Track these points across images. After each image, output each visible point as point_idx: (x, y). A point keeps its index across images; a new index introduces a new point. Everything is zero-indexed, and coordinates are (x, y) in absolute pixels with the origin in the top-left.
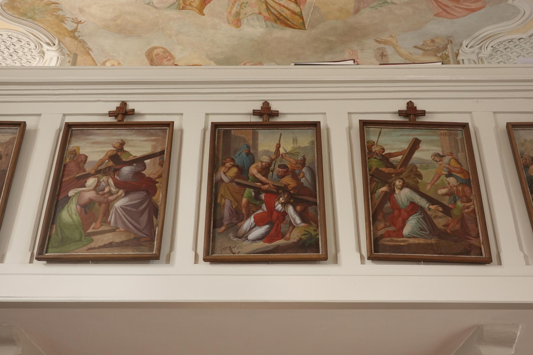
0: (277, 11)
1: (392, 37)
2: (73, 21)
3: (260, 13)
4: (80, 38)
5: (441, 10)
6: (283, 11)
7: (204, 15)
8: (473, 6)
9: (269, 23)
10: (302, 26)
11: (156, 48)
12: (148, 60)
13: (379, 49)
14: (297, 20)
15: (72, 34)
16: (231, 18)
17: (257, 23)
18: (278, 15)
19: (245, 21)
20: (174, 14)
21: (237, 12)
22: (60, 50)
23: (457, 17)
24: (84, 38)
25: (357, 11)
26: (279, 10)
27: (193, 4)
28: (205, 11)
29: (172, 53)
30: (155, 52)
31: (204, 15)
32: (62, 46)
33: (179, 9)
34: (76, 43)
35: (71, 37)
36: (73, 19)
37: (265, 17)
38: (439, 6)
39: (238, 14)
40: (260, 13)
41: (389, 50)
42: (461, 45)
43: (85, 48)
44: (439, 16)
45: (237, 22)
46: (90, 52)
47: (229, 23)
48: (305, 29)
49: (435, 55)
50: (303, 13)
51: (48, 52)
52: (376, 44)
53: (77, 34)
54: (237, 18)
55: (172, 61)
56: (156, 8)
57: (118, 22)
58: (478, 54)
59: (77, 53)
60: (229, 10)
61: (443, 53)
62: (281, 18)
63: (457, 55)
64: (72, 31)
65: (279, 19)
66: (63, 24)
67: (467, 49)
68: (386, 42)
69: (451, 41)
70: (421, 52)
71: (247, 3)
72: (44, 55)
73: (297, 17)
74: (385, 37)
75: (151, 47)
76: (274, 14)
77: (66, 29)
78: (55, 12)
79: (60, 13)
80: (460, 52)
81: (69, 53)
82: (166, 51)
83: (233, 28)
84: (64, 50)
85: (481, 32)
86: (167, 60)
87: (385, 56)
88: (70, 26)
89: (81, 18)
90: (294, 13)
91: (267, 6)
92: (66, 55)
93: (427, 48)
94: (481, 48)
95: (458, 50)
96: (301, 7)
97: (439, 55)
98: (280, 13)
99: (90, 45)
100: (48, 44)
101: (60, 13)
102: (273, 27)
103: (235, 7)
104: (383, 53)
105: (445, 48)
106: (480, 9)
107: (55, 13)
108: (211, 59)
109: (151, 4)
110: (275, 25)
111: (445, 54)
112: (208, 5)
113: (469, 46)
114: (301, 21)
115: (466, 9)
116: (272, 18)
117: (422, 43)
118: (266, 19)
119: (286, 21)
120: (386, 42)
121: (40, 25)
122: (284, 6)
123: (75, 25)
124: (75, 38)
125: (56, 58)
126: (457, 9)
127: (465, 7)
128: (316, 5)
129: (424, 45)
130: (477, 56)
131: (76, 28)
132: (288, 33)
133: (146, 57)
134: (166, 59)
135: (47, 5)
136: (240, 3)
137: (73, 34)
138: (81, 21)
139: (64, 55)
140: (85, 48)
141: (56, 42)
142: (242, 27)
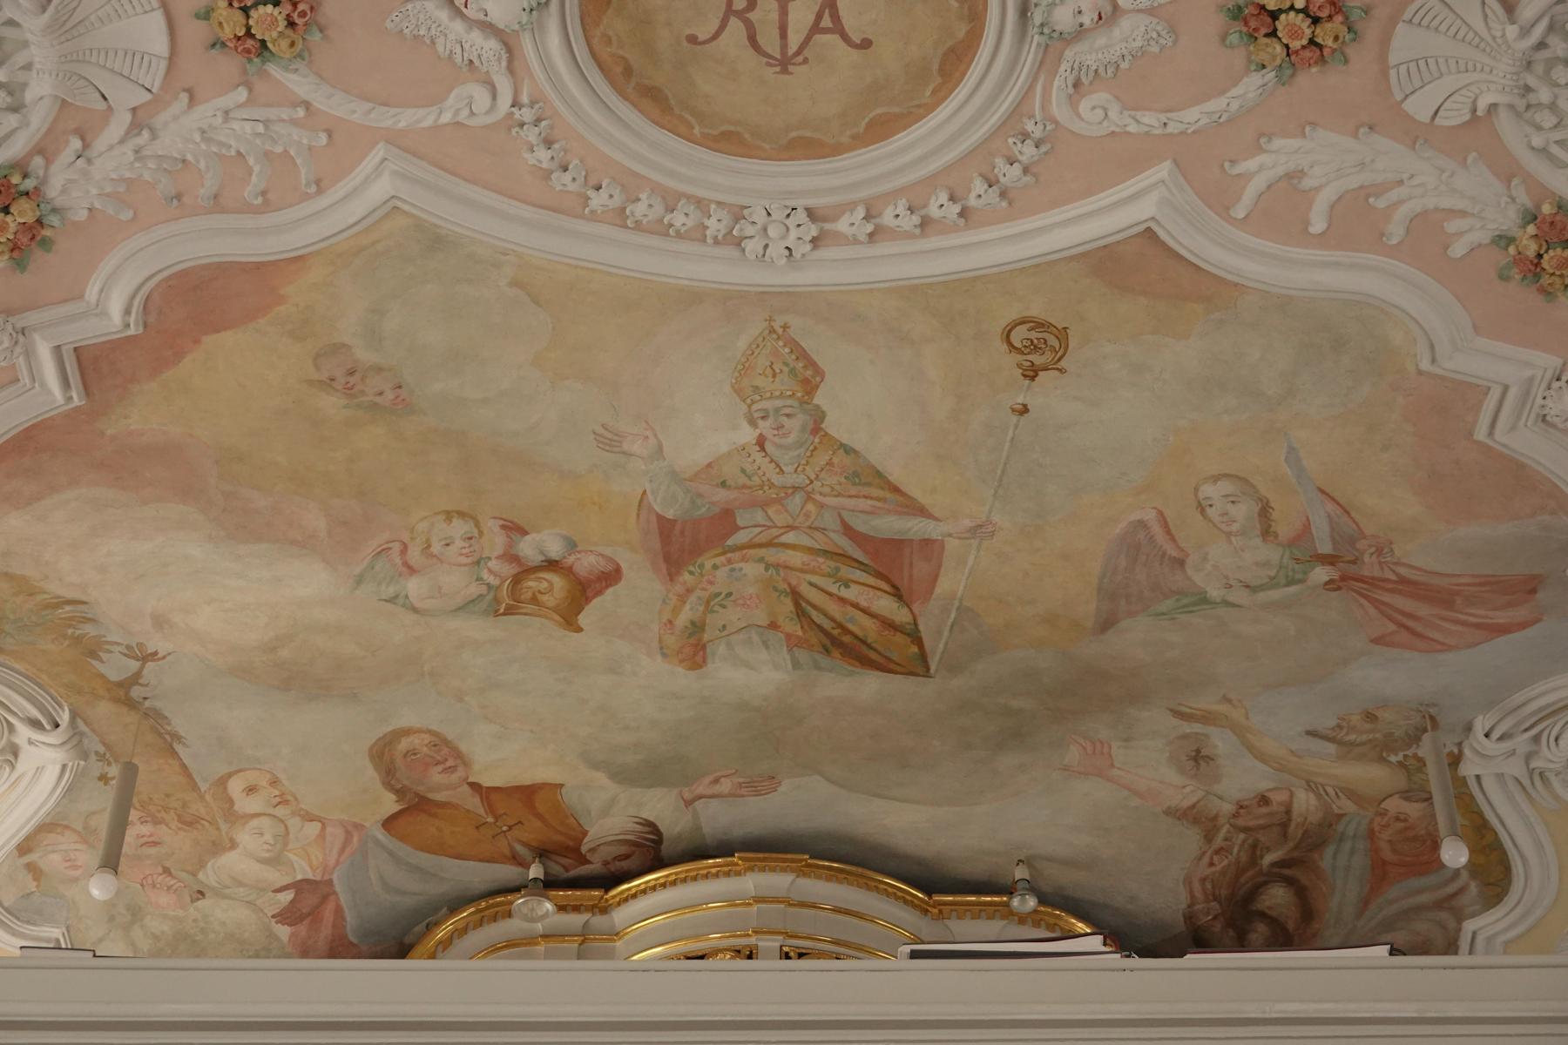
0: (833, 620)
1: (1229, 701)
2: (129, 653)
3: (773, 626)
4: (147, 704)
5: (1392, 627)
6: (852, 620)
7: (579, 630)
8: (1501, 618)
9: (802, 655)
10: (919, 666)
11: (407, 732)
12: (377, 768)
13: (1185, 737)
14: (900, 648)
15: (122, 693)
16: (672, 641)
17: (764, 655)
18: (836, 632)
19: (722, 649)
20: (477, 628)
21: (693, 623)
22: (74, 741)
23: (1449, 648)
24: (158, 704)
25: (1106, 624)
26: (838, 616)
27: (544, 598)
28: (583, 619)
29: (464, 747)
30: (404, 744)
31: (579, 630)
32: (83, 727)
33: (496, 614)
34: (131, 718)
35: (116, 700)
36: (128, 647)
37: (788, 636)
38: (1381, 612)
39: (697, 627)
40: (773, 626)
41: (1221, 742)
42: (1469, 728)
43: (160, 735)
44: (1387, 645)
45: (694, 649)
46: (176, 746)
47: (664, 655)
48: (926, 673)
49: (1382, 760)
50: (921, 628)
51: (32, 748)
52: (1176, 722)
53: (136, 692)
54: (692, 640)
55: (460, 773)
56: (415, 610)
57: (284, 653)
58: (1529, 757)
59: (136, 761)
60: (666, 617)
61: (1409, 753)
62: (847, 639)
63: (1455, 760)
64: (120, 684)
65: (836, 643)
66: (94, 662)
67: (1490, 747)
68: (1207, 718)
69: (1432, 718)
70: (1331, 748)
71: (729, 594)
72: (16, 755)
73: (899, 638)
74: (1206, 702)
75: (390, 728)
76: (821, 628)
77: (102, 676)
78: (70, 626)
79: (90, 630)
80: (1467, 751)
81: (102, 749)
82: (440, 741)
83: (680, 670)
84: (86, 741)
85: (1533, 693)
86: (445, 770)
87: (1209, 758)
88: (115, 667)
89: (156, 643)
90: (889, 625)
91: (797, 605)
92: (93, 757)
93: (1352, 737)
94: (1536, 739)
95: (1460, 744)
96: (916, 607)
97: (1393, 759)
98: (840, 626)
99: (179, 724)
100: (35, 724)
101: (90, 630)
102: (817, 667)
103: (687, 607)
104: (1198, 751)
105: (1414, 738)
106: (1523, 626)
107: (70, 631)
108: (596, 766)
109: (401, 601)
110: (824, 661)
111: (1415, 756)
112: (596, 602)
113: (1495, 735)
114: (915, 649)
115: (1477, 626)
116: (814, 641)
117: (1333, 722)
118: (793, 643)
119: (864, 649)
120: (1207, 718)
121: (17, 666)
122: (856, 606)
123: (134, 665)
124: (131, 704)
125: (58, 768)
126: (1446, 625)
127: (1472, 619)
128: (966, 603)
129: (1340, 727)
130: (1527, 764)
131: (138, 675)
132: (871, 685)
133: (372, 758)
134: (440, 768)
135: (47, 606)
136: (705, 595)
137: (124, 693)
138: (156, 653)
139: (85, 756)
140: (160, 735)
141: (64, 717)
142: (710, 666)
